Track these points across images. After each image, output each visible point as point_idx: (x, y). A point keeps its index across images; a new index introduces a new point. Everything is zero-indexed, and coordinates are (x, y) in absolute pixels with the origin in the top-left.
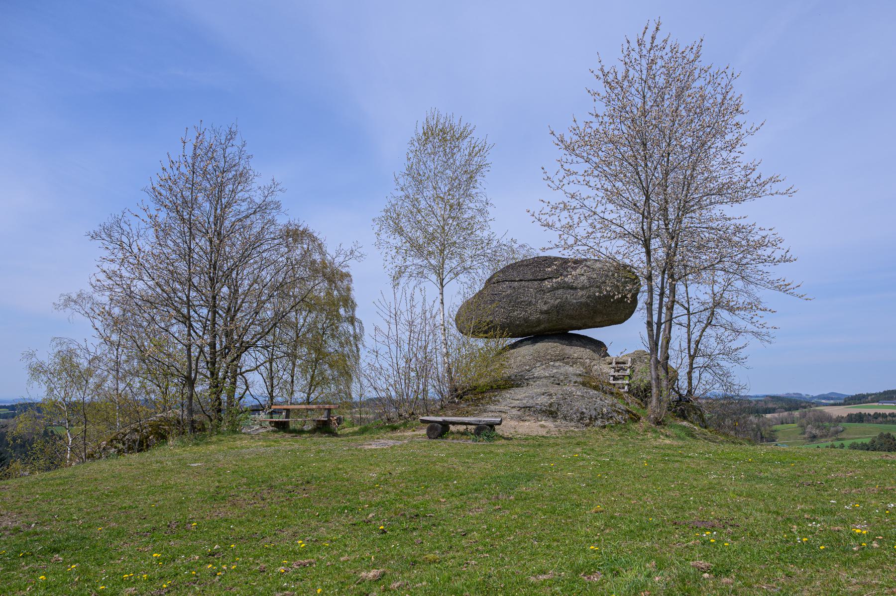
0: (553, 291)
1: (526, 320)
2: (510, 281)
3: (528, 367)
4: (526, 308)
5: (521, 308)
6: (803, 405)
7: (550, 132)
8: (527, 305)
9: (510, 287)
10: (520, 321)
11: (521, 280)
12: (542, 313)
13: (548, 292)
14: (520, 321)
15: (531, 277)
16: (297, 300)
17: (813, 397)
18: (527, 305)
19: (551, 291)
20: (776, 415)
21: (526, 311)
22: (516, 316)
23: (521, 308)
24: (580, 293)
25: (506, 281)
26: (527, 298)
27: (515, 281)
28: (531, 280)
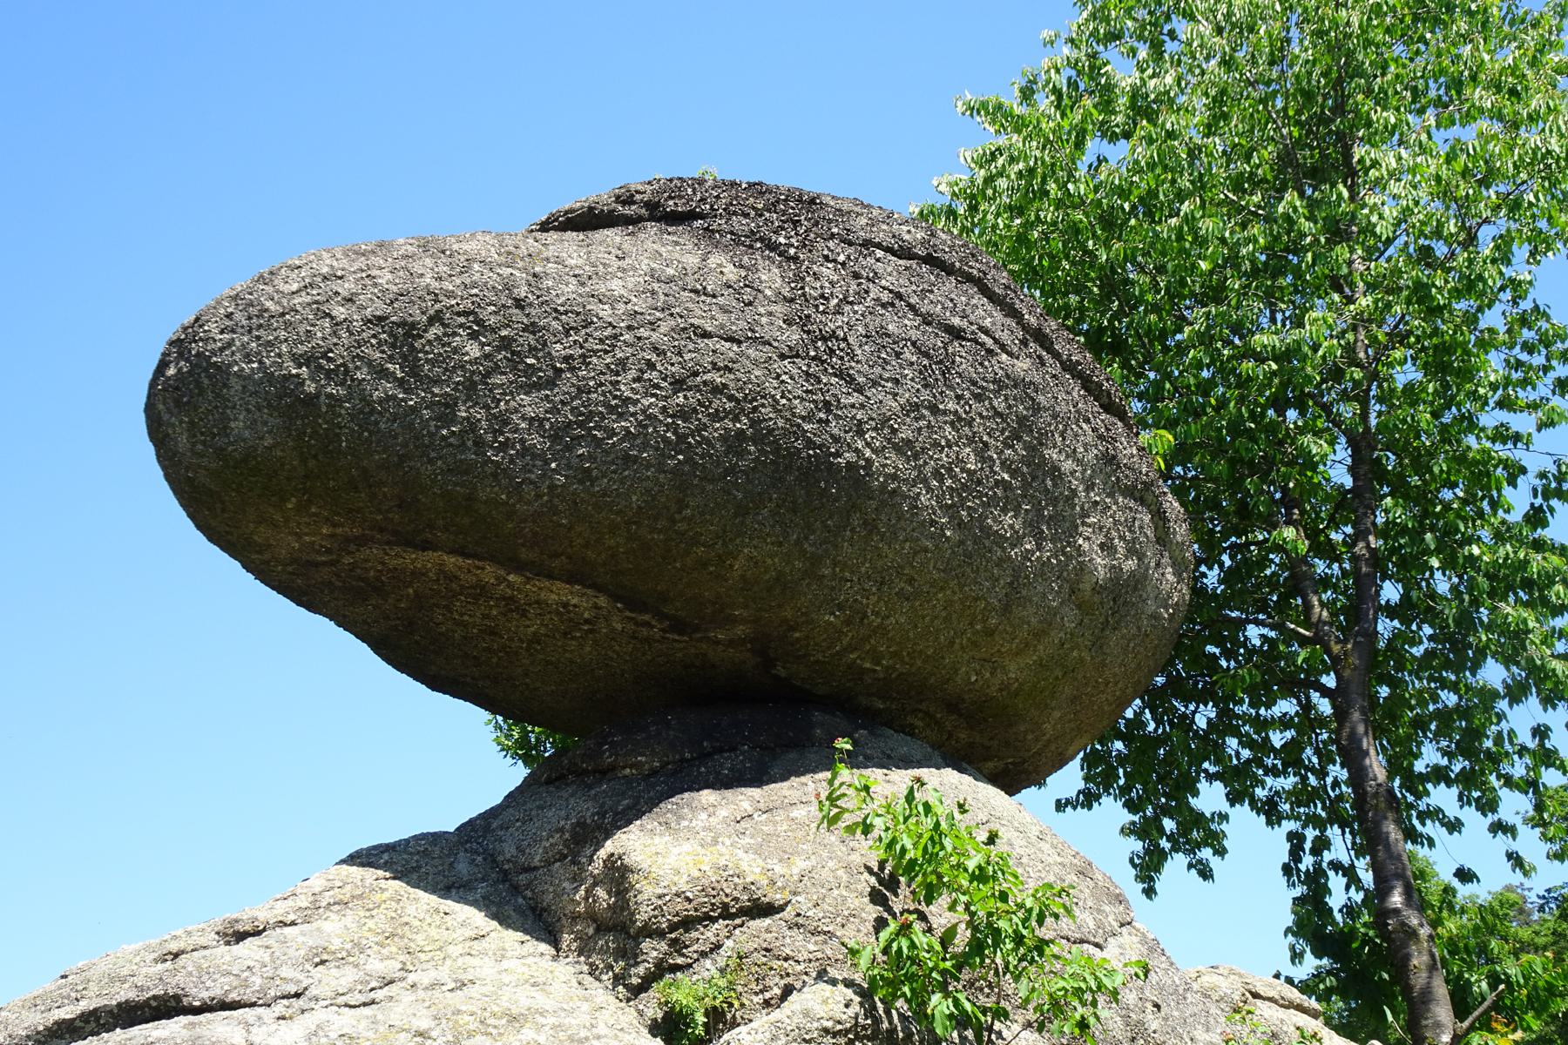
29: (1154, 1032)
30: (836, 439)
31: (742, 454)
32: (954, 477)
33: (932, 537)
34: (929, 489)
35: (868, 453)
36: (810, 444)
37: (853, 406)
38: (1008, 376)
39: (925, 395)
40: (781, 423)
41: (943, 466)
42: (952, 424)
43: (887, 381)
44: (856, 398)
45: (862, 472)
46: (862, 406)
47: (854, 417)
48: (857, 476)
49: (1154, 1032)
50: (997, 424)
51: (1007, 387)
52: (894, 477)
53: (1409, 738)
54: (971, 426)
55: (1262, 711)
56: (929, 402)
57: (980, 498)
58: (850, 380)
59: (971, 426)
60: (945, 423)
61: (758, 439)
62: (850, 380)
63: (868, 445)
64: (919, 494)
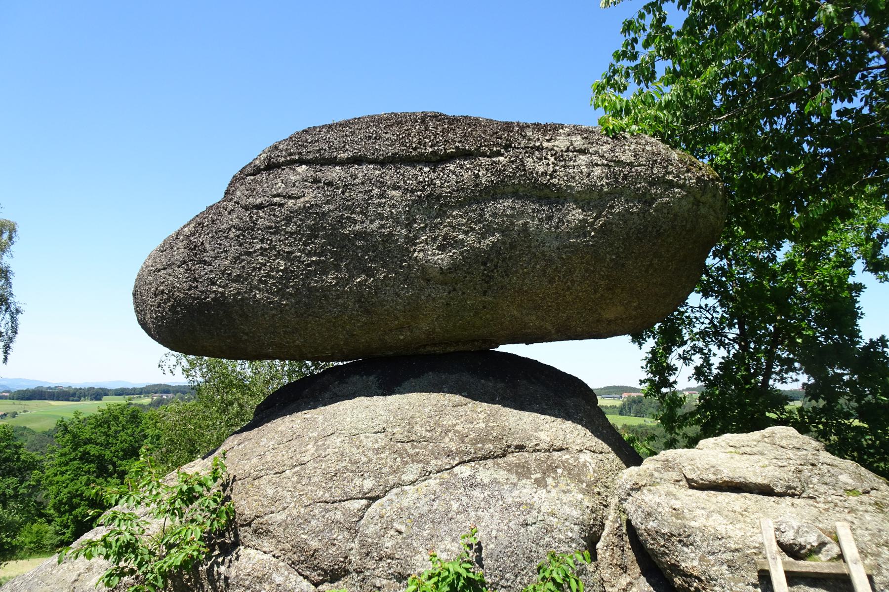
11: (357, 160)
15: (397, 148)
26: (376, 224)
27: (333, 162)
29: (387, 548)
30: (202, 292)
31: (178, 313)
32: (273, 277)
33: (274, 308)
34: (260, 290)
35: (221, 290)
36: (194, 299)
37: (206, 274)
38: (291, 212)
39: (241, 249)
40: (182, 295)
41: (262, 276)
42: (261, 254)
43: (222, 253)
44: (208, 268)
45: (221, 299)
46: (211, 271)
47: (208, 279)
48: (220, 301)
49: (387, 548)
50: (295, 238)
51: (293, 217)
52: (239, 293)
53: (713, 291)
54: (275, 249)
55: (824, 238)
56: (244, 252)
57: (298, 277)
58: (205, 263)
59: (275, 249)
60: (257, 256)
61: (179, 305)
62: (205, 263)
63: (220, 286)
64: (255, 294)
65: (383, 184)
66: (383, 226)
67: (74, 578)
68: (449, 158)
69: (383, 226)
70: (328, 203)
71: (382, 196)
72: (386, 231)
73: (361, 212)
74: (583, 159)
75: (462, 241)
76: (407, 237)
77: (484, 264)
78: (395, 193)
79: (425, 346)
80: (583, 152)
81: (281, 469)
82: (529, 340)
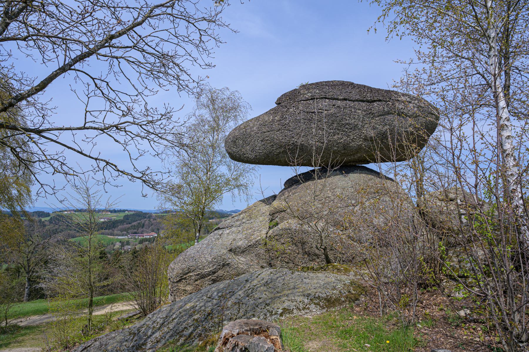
0: (383, 115)
1: (346, 147)
2: (332, 99)
3: (353, 202)
4: (350, 132)
5: (344, 131)
6: (225, 215)
7: (230, 27)
8: (351, 129)
9: (334, 105)
10: (338, 147)
11: (345, 99)
12: (365, 139)
13: (378, 116)
14: (338, 147)
15: (358, 97)
16: (61, 36)
17: (228, 212)
18: (351, 129)
19: (381, 115)
20: (214, 220)
21: (348, 136)
22: (335, 141)
23: (344, 131)
24: (410, 121)
25: (326, 98)
26: (353, 121)
27: (338, 99)
28: (357, 101)
39: (306, 127)
44: (291, 133)
65: (355, 108)
66: (355, 122)
67: (230, 243)
68: (375, 101)
69: (355, 122)
70: (338, 113)
71: (355, 112)
72: (356, 123)
73: (349, 117)
74: (411, 105)
75: (378, 128)
76: (362, 126)
77: (383, 136)
78: (359, 111)
79: (350, 162)
80: (410, 102)
81: (321, 199)
82: (365, 164)
